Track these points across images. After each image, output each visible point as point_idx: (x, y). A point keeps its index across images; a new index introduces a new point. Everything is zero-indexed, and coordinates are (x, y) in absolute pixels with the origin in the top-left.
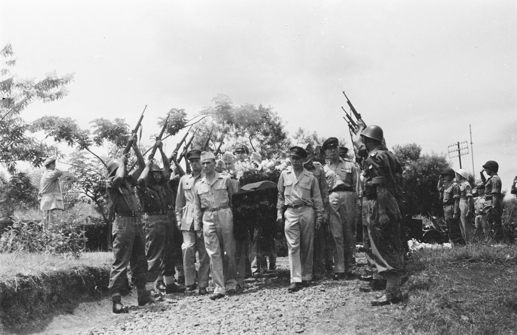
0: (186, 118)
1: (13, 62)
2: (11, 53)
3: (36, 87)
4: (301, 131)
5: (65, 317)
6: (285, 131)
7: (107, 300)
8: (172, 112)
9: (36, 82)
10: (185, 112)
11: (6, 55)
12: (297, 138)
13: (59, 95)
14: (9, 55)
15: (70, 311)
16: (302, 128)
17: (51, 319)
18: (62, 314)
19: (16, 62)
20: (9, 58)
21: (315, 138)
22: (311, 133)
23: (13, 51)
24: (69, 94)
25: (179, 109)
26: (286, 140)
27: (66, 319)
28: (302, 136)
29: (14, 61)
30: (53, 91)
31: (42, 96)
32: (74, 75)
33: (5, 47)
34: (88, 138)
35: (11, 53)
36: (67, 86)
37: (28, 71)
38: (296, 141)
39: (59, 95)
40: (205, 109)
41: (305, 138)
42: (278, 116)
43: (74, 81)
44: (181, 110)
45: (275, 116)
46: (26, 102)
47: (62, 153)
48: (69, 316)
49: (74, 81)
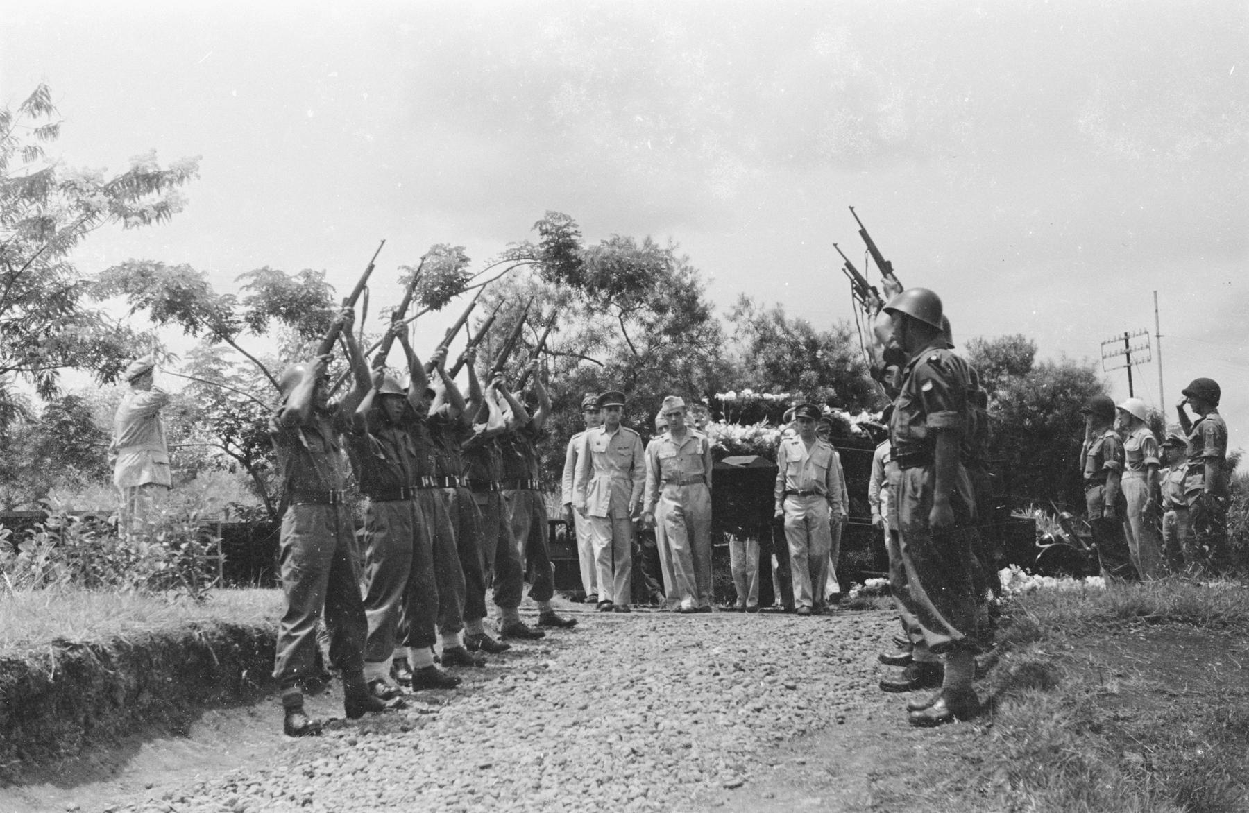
0: (467, 270)
1: (51, 131)
2: (48, 108)
3: (108, 190)
4: (746, 303)
5: (170, 743)
6: (708, 301)
7: (269, 703)
8: (434, 253)
9: (108, 178)
10: (466, 253)
11: (36, 112)
12: (734, 319)
13: (162, 209)
14: (44, 112)
15: (180, 730)
16: (747, 295)
17: (136, 749)
18: (163, 735)
19: (60, 130)
20: (43, 120)
21: (779, 320)
22: (770, 306)
23: (53, 102)
24: (186, 207)
25: (452, 246)
26: (707, 324)
27: (169, 748)
28: (746, 315)
29: (55, 127)
30: (149, 199)
31: (124, 213)
32: (200, 163)
33: (35, 94)
34: (231, 314)
35: (48, 108)
36: (184, 190)
37: (88, 150)
38: (734, 325)
39: (162, 209)
40: (515, 246)
41: (754, 318)
42: (689, 264)
43: (198, 176)
44: (456, 249)
45: (683, 266)
46: (84, 227)
47: (169, 350)
48: (179, 742)
49: (198, 176)
